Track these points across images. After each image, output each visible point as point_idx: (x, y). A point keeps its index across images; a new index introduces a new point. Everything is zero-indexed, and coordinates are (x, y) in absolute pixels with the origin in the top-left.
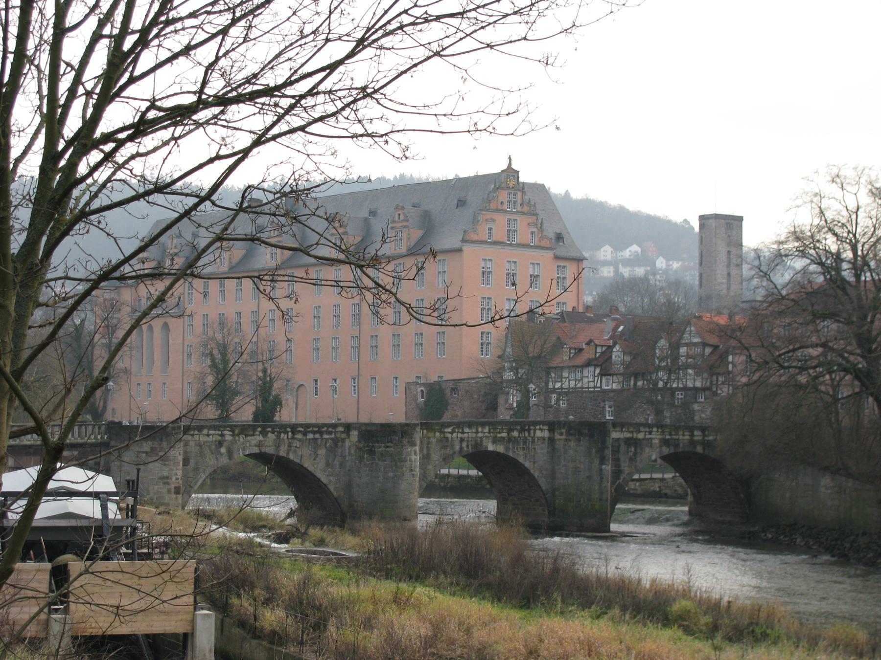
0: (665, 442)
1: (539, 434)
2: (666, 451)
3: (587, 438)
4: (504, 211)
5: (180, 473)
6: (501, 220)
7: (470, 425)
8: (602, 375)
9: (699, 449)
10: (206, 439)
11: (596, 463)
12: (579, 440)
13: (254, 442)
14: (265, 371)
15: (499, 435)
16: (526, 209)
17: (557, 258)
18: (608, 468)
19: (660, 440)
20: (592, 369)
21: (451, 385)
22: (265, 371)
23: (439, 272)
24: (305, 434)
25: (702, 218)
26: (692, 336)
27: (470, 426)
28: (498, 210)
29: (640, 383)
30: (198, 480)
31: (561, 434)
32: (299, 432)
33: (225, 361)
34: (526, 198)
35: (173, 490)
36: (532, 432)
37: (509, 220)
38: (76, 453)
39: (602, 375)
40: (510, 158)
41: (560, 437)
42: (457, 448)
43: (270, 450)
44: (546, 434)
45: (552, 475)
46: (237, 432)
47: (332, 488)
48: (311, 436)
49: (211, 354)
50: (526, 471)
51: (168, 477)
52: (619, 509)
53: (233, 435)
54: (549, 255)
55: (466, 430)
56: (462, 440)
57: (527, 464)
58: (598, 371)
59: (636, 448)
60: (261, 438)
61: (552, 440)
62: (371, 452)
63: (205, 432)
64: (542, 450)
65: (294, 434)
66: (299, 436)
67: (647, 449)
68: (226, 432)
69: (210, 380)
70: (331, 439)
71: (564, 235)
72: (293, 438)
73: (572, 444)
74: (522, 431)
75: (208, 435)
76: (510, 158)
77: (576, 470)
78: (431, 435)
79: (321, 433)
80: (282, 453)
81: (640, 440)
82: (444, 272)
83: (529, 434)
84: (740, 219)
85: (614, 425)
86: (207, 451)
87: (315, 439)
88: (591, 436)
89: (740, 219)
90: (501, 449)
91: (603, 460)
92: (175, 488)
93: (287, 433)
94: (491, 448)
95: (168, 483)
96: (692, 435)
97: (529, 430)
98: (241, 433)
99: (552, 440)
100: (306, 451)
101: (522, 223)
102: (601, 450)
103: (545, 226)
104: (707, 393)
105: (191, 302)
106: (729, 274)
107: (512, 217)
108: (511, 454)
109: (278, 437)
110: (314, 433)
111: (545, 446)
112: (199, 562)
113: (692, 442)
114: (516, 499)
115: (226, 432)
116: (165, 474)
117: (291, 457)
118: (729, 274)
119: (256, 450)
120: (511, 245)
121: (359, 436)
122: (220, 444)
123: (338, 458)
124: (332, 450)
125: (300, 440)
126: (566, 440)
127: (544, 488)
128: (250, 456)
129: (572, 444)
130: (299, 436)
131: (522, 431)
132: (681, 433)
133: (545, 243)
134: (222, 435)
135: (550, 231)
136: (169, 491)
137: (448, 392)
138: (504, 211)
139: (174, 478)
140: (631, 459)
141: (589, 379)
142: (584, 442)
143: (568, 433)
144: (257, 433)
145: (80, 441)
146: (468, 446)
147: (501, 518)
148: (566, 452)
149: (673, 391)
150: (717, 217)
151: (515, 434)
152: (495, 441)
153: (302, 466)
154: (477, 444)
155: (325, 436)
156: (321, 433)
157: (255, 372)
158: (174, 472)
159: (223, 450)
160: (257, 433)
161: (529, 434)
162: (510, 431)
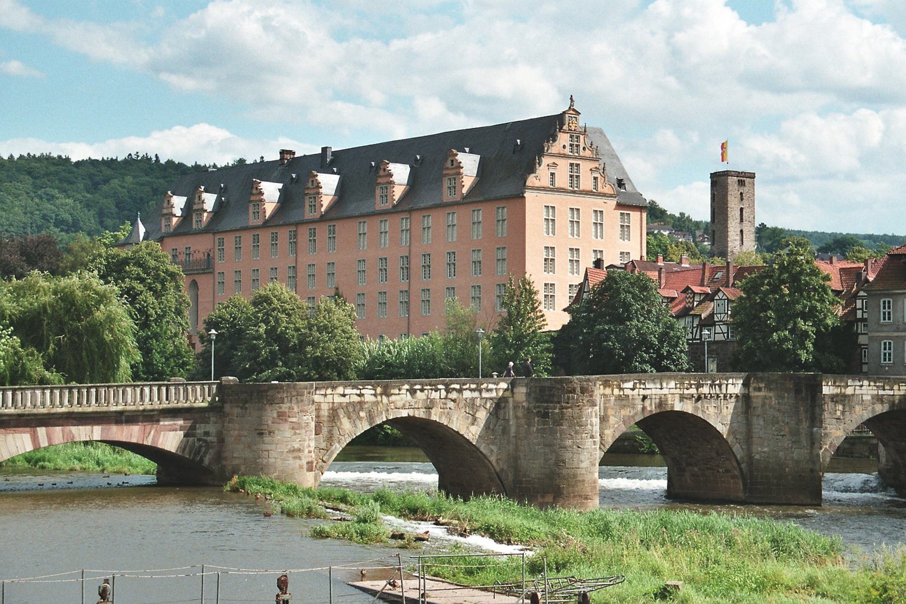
3: (792, 394)
5: (313, 444)
10: (342, 400)
11: (805, 425)
15: (686, 392)
19: (873, 397)
23: (498, 221)
30: (332, 453)
31: (760, 389)
32: (454, 389)
35: (305, 466)
36: (724, 387)
37: (571, 165)
40: (571, 98)
43: (420, 414)
47: (493, 459)
51: (299, 450)
56: (644, 398)
59: (844, 405)
70: (491, 399)
71: (625, 182)
75: (344, 395)
76: (571, 98)
81: (849, 396)
82: (503, 220)
83: (721, 390)
87: (473, 399)
90: (688, 407)
92: (308, 463)
94: (678, 407)
95: (300, 458)
103: (607, 168)
106: (742, 231)
107: (575, 162)
108: (700, 415)
114: (696, 469)
116: (296, 446)
118: (742, 231)
120: (574, 192)
123: (500, 422)
125: (454, 401)
127: (738, 457)
130: (454, 395)
132: (896, 387)
133: (608, 190)
139: (306, 451)
144: (404, 391)
145: (187, 405)
146: (651, 404)
155: (485, 395)
158: (306, 443)
160: (404, 391)
161: (721, 390)
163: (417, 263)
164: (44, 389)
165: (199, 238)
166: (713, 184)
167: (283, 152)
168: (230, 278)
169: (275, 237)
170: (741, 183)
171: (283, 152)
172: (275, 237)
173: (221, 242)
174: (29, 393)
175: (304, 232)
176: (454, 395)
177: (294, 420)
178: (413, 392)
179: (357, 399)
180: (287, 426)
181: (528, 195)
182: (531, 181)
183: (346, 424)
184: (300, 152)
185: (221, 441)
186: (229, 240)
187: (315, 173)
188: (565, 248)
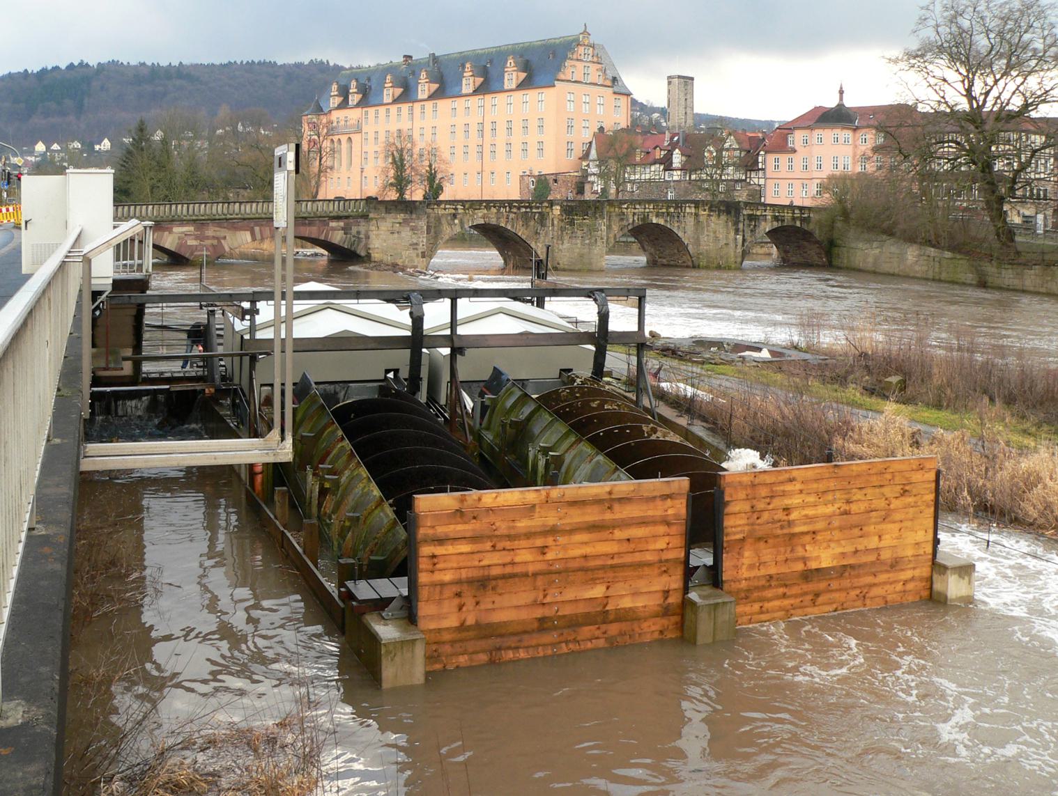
1: (688, 210)
2: (776, 225)
4: (581, 60)
6: (580, 65)
7: (640, 202)
8: (665, 170)
9: (798, 224)
10: (443, 212)
11: (732, 233)
12: (719, 216)
13: (480, 215)
14: (430, 166)
16: (595, 59)
17: (615, 93)
18: (740, 237)
20: (658, 166)
21: (553, 177)
22: (430, 166)
24: (519, 208)
25: (554, 86)
26: (730, 142)
27: (640, 204)
28: (578, 60)
29: (693, 177)
33: (402, 160)
34: (596, 52)
38: (342, 224)
39: (665, 170)
41: (703, 213)
42: (631, 220)
43: (494, 221)
44: (693, 210)
45: (697, 242)
46: (467, 206)
48: (524, 210)
49: (393, 154)
50: (678, 239)
51: (417, 244)
52: (151, 314)
53: (464, 209)
54: (610, 90)
55: (638, 206)
56: (634, 214)
57: (680, 234)
58: (662, 167)
60: (485, 211)
61: (697, 215)
62: (572, 223)
63: (443, 206)
64: (690, 221)
65: (510, 208)
66: (515, 210)
67: (763, 223)
72: (510, 212)
74: (676, 208)
77: (716, 239)
78: (612, 210)
79: (531, 208)
84: (692, 79)
85: (746, 204)
86: (444, 221)
88: (728, 213)
89: (692, 79)
90: (661, 222)
91: (737, 231)
94: (654, 221)
96: (794, 213)
97: (681, 207)
98: (471, 207)
101: (593, 68)
102: (736, 223)
104: (743, 183)
105: (367, 123)
109: (498, 210)
110: (526, 207)
113: (794, 219)
119: (482, 222)
122: (455, 216)
126: (709, 215)
128: (476, 227)
129: (713, 218)
133: (609, 83)
135: (610, 74)
136: (417, 255)
137: (551, 181)
138: (581, 60)
140: (752, 231)
141: (654, 172)
142: (724, 217)
143: (710, 210)
148: (708, 226)
149: (718, 182)
150: (679, 77)
151: (672, 210)
154: (645, 217)
156: (531, 208)
162: (668, 207)
163: (488, 127)
166: (669, 83)
168: (371, 136)
169: (399, 110)
172: (399, 110)
173: (367, 113)
175: (417, 106)
176: (514, 210)
185: (368, 237)
186: (372, 111)
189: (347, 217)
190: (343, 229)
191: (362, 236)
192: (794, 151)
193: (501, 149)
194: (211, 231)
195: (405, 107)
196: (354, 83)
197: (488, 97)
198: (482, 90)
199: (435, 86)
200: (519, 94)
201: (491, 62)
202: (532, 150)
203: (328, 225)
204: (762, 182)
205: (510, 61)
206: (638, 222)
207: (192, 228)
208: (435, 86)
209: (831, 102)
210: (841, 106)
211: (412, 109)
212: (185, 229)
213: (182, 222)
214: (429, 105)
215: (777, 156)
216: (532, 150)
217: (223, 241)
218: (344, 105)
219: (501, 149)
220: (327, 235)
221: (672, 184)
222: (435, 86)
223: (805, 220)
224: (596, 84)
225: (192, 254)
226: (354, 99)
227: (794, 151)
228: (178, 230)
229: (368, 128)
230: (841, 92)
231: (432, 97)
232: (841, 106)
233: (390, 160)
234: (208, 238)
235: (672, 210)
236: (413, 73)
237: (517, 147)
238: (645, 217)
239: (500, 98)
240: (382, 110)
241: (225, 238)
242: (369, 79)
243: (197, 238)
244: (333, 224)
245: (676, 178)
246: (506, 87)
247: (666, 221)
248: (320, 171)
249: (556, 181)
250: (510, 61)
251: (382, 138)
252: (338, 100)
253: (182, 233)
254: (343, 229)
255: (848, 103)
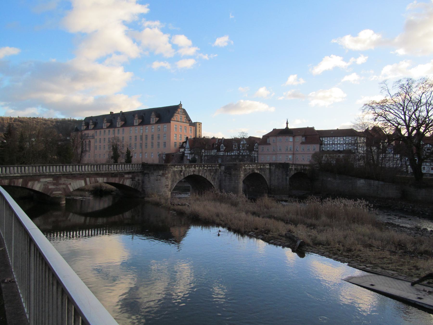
0: (295, 169)
2: (296, 172)
9: (302, 171)
29: (228, 154)
38: (130, 176)
39: (217, 151)
53: (185, 168)
57: (264, 177)
63: (176, 167)
64: (268, 171)
68: (183, 167)
69: (112, 153)
73: (277, 170)
74: (263, 166)
75: (177, 168)
80: (200, 175)
84: (200, 124)
87: (210, 169)
89: (200, 124)
90: (258, 172)
93: (202, 167)
94: (256, 172)
98: (188, 167)
99: (270, 169)
100: (207, 174)
110: (210, 167)
111: (268, 171)
112: (358, 244)
115: (183, 167)
116: (167, 184)
117: (203, 176)
121: (225, 168)
124: (215, 173)
131: (263, 166)
134: (182, 168)
147: (48, 187)
152: (257, 169)
153: (206, 179)
155: (213, 168)
157: (125, 150)
159: (182, 174)
162: (261, 166)
163: (144, 137)
164: (69, 165)
165: (91, 131)
167: (111, 112)
168: (98, 140)
169: (109, 131)
170: (199, 125)
171: (111, 112)
172: (109, 131)
173: (96, 132)
174: (55, 167)
175: (116, 129)
176: (205, 168)
177: (166, 176)
178: (195, 167)
179: (180, 169)
180: (164, 178)
181: (172, 122)
182: (172, 119)
183: (178, 177)
184: (115, 112)
185: (143, 182)
186: (98, 131)
187: (334, 41)
188: (177, 134)
189: (133, 173)
190: (131, 178)
191: (140, 182)
192: (270, 144)
193: (149, 145)
194: (63, 180)
195: (112, 130)
196: (91, 121)
197: (144, 126)
198: (141, 124)
199: (123, 122)
200: (139, 127)
201: (144, 114)
202: (162, 146)
203: (124, 176)
204: (256, 155)
205: (153, 114)
206: (251, 172)
207: (51, 179)
208: (123, 123)
209: (284, 127)
210: (287, 127)
211: (114, 131)
212: (48, 180)
213: (46, 176)
214: (121, 129)
215: (263, 146)
216: (162, 146)
217: (69, 186)
218: (87, 129)
219: (149, 145)
220: (123, 182)
221: (246, 157)
222: (123, 123)
223: (305, 170)
224: (184, 122)
225: (51, 193)
226: (91, 127)
227: (270, 144)
228: (43, 180)
229: (97, 137)
230: (287, 123)
231: (122, 126)
232: (287, 127)
233: (112, 148)
234: (61, 184)
235: (262, 167)
236: (114, 118)
237: (155, 144)
238: (253, 170)
239: (148, 127)
240: (102, 131)
241: (70, 184)
242: (96, 120)
243: (54, 184)
244: (126, 176)
245: (222, 154)
246: (151, 123)
247: (260, 172)
248: (82, 152)
249: (173, 156)
250: (153, 114)
251: (107, 140)
252: (85, 127)
253: (46, 182)
254: (131, 178)
255: (290, 127)
